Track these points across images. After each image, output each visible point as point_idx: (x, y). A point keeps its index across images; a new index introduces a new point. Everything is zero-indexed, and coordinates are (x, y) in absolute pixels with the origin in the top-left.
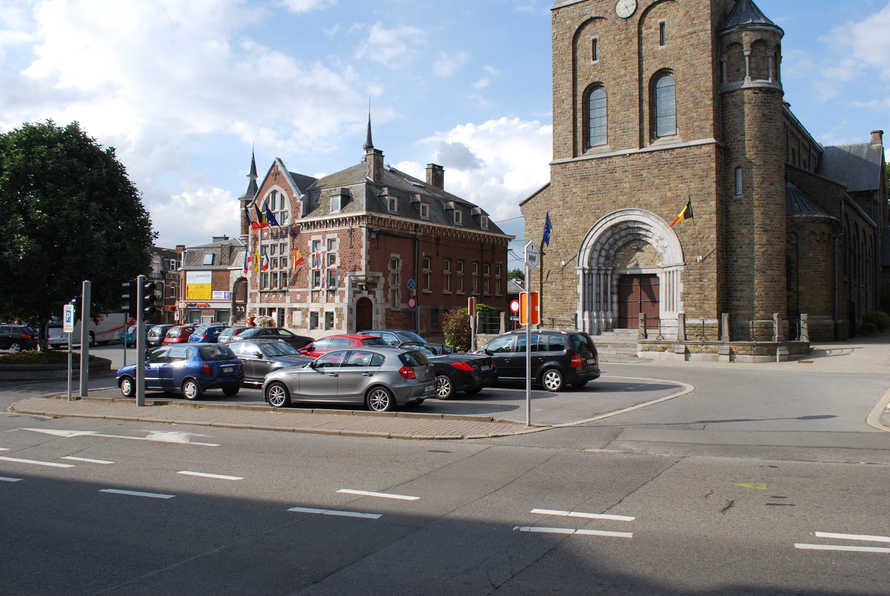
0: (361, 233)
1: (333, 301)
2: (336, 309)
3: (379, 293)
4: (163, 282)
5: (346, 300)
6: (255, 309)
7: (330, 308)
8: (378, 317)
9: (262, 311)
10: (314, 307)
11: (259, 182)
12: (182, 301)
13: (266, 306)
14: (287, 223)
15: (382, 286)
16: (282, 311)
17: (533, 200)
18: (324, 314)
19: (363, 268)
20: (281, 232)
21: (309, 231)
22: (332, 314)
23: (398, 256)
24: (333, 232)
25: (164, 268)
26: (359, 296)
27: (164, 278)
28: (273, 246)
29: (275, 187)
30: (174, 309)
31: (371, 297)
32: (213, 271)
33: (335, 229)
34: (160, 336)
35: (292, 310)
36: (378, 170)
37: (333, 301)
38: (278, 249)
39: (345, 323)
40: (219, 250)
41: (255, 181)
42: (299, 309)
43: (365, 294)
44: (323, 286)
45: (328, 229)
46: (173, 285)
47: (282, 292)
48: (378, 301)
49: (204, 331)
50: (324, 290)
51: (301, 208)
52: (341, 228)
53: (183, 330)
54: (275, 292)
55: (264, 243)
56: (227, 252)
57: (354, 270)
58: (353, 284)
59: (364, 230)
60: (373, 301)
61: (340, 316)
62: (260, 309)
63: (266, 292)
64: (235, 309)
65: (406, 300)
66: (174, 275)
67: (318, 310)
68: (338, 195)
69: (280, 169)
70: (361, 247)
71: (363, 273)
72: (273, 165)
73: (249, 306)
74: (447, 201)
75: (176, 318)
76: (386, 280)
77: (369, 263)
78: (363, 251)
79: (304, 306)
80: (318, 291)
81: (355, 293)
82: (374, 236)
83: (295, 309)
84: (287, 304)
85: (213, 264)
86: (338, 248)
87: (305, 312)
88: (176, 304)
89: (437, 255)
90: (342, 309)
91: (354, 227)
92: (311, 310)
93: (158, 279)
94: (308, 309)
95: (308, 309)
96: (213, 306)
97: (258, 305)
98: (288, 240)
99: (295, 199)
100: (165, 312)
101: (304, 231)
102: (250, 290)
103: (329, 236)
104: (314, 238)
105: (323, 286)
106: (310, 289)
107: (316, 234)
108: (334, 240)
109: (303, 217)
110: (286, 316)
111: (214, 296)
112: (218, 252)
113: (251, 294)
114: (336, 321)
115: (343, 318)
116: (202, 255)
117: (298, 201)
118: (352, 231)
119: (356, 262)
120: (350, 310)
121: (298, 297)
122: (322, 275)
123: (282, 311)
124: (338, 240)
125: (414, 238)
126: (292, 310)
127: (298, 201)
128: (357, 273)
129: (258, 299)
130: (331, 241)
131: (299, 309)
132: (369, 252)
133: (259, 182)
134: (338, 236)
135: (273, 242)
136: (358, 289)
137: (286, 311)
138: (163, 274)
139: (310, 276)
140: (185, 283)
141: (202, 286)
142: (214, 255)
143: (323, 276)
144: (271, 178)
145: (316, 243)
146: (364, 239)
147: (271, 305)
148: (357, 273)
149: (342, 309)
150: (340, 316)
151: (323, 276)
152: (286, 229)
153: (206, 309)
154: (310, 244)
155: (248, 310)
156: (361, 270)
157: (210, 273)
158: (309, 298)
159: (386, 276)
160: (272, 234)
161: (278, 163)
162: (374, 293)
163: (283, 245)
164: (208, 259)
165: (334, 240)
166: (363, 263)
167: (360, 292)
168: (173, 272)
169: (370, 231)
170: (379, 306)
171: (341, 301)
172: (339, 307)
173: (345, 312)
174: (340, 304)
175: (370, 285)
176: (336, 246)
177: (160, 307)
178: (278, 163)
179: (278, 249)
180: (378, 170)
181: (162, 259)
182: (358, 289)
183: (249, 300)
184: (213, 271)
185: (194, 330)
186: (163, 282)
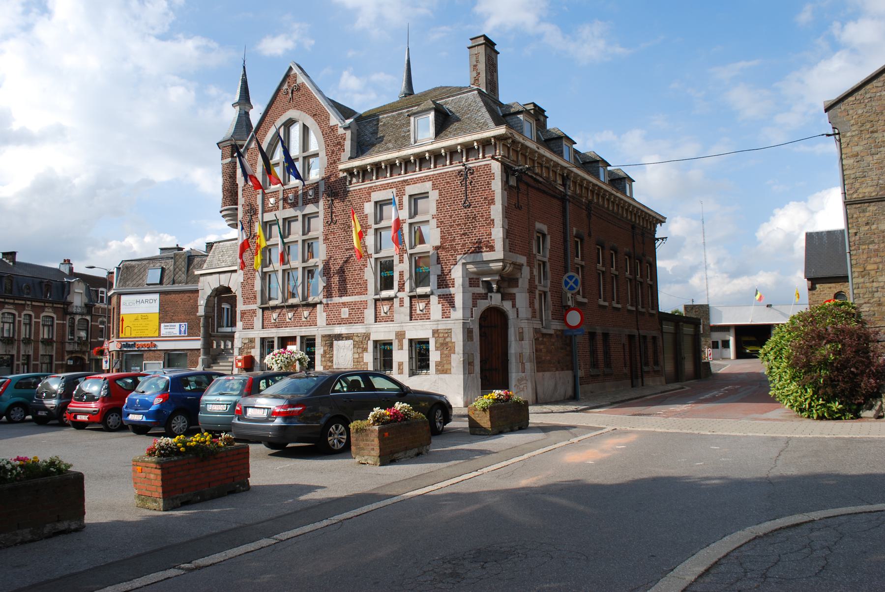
0: (491, 176)
1: (426, 316)
2: (435, 332)
3: (522, 298)
4: (88, 318)
5: (458, 314)
6: (252, 341)
7: (419, 330)
8: (520, 347)
9: (267, 345)
10: (382, 332)
11: (255, 117)
12: (114, 339)
13: (274, 333)
14: (315, 175)
15: (527, 286)
16: (309, 343)
17: (858, 95)
18: (406, 343)
19: (499, 245)
20: (305, 194)
21: (367, 184)
22: (427, 342)
23: (544, 228)
24: (420, 181)
25: (90, 299)
26: (483, 304)
27: (89, 312)
28: (288, 221)
29: (292, 114)
30: (102, 353)
31: (507, 306)
32: (161, 293)
33: (425, 173)
34: (61, 397)
35: (331, 340)
36: (492, 75)
37: (426, 316)
38: (297, 227)
39: (457, 360)
40: (171, 262)
41: (247, 114)
42: (348, 337)
43: (496, 299)
44: (401, 288)
45: (408, 177)
46: (102, 323)
47: (308, 305)
48: (520, 314)
49: (162, 385)
50: (405, 295)
51: (348, 144)
52: (441, 170)
53: (112, 384)
54: (292, 307)
55: (268, 217)
56: (183, 264)
57: (478, 250)
58: (472, 281)
59: (496, 167)
60: (511, 314)
61: (445, 346)
62: (263, 340)
63: (274, 308)
64: (207, 346)
65: (561, 311)
66: (104, 309)
67: (391, 336)
68: (430, 109)
69: (301, 79)
70: (492, 202)
71: (499, 253)
72: (287, 76)
73: (240, 334)
74: (511, 187)
75: (105, 366)
76: (531, 273)
77: (508, 234)
78: (497, 211)
79: (358, 329)
80: (390, 299)
81: (476, 297)
82: (513, 182)
83: (339, 337)
84: (320, 328)
85: (161, 283)
86: (433, 210)
87: (360, 342)
88: (105, 346)
89: (590, 235)
90: (449, 332)
91: (472, 164)
92: (373, 337)
93: (82, 314)
94: (367, 336)
95: (367, 336)
96: (161, 346)
97: (258, 333)
98: (321, 207)
99: (333, 129)
100: (90, 360)
101: (356, 186)
102: (240, 307)
103: (411, 190)
104: (377, 196)
105: (401, 288)
106: (371, 296)
107: (381, 189)
108: (425, 195)
109: (350, 158)
110: (319, 351)
111: (164, 331)
112: (170, 265)
113: (243, 313)
114: (434, 356)
115: (452, 350)
116: (145, 269)
117: (341, 131)
118: (466, 175)
119: (479, 233)
120: (468, 333)
121: (345, 313)
122: (398, 268)
123: (309, 343)
124: (434, 195)
125: (563, 199)
126: (331, 340)
127: (341, 131)
128: (487, 256)
129: (258, 322)
130: (415, 199)
131: (348, 337)
132: (508, 212)
133: (255, 117)
134: (434, 187)
135: (290, 212)
136: (481, 290)
137: (318, 341)
138: (89, 308)
139: (370, 275)
140: (119, 313)
141: (145, 317)
142: (163, 270)
143: (402, 268)
144: (282, 99)
145: (380, 205)
146: (497, 185)
147: (286, 332)
148: (487, 256)
149: (449, 332)
150: (445, 346)
151: (402, 268)
152: (316, 186)
153: (151, 351)
154: (369, 208)
155: (238, 343)
156: (492, 248)
157: (157, 297)
158: (369, 313)
159: (530, 264)
160: (285, 200)
161: (296, 70)
162: (512, 298)
163: (307, 218)
164: (153, 276)
165: (425, 195)
166: (497, 234)
167: (485, 297)
168: (102, 305)
169: (507, 170)
170: (524, 325)
171: (445, 315)
172: (441, 327)
173: (458, 338)
174: (445, 322)
175: (507, 281)
176: (429, 207)
177: (84, 353)
178: (296, 70)
179: (297, 227)
180: (492, 75)
181: (88, 289)
182: (481, 290)
183: (239, 324)
184: (161, 293)
185: (136, 383)
186: (88, 318)
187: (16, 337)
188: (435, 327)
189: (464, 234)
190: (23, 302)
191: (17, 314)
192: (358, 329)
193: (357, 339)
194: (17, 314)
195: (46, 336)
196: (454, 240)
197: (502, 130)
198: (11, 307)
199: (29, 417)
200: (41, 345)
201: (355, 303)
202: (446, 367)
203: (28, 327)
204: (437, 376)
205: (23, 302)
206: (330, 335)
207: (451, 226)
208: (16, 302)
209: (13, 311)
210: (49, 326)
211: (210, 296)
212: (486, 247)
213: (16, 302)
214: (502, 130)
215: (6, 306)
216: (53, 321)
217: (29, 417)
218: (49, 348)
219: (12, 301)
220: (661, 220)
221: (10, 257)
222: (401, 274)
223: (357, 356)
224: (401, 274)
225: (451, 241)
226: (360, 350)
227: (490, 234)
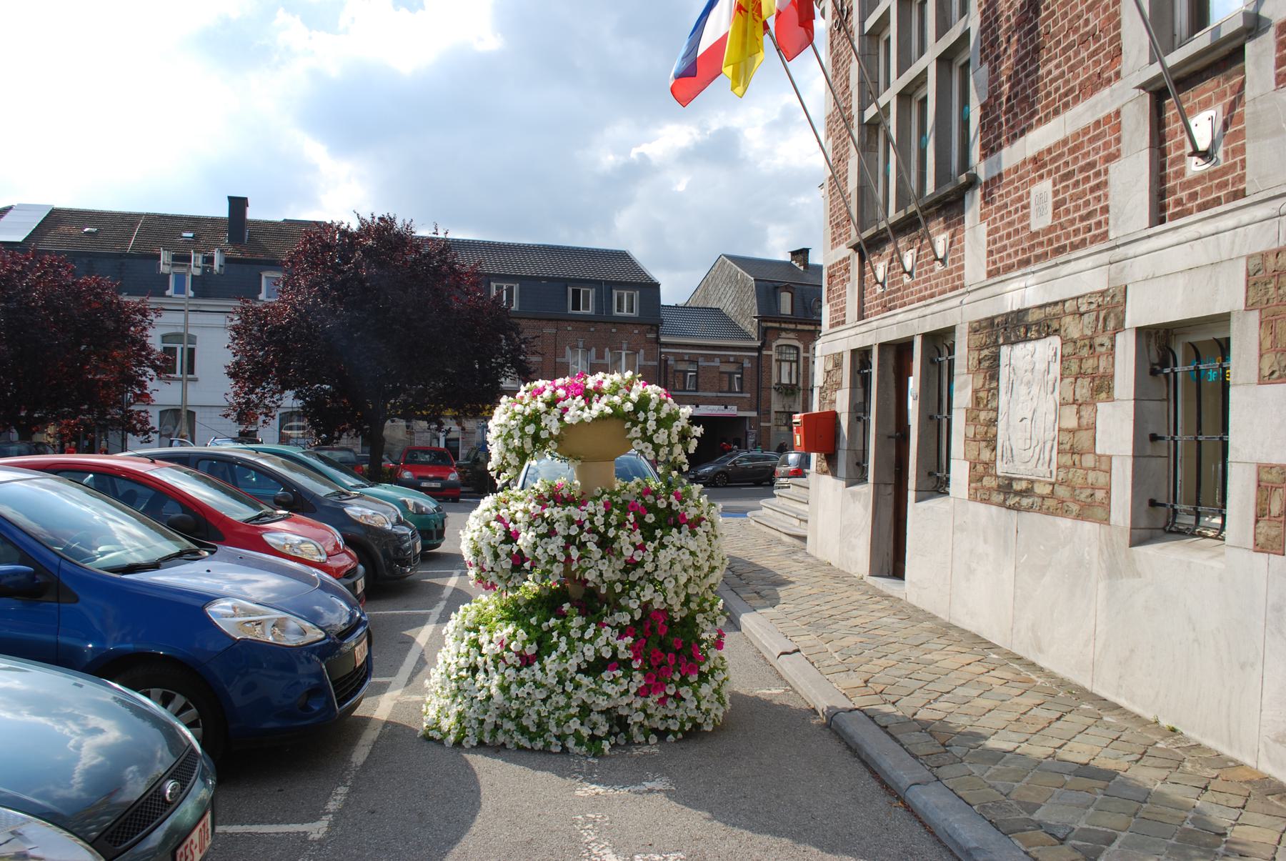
79: (1081, 276)
92: (1147, 308)
94: (1110, 306)
95: (1110, 306)
187: (801, 385)
190: (777, 325)
191: (801, 346)
192: (1081, 276)
193: (1074, 329)
194: (801, 346)
195: (785, 380)
198: (792, 335)
199: (407, 475)
200: (774, 394)
201: (1072, 145)
203: (794, 365)
205: (777, 325)
206: (991, 321)
208: (799, 327)
209: (796, 343)
210: (791, 362)
213: (799, 327)
215: (783, 334)
216: (798, 354)
217: (407, 475)
218: (788, 401)
219: (792, 326)
221: (801, 257)
223: (1071, 422)
226: (1083, 389)
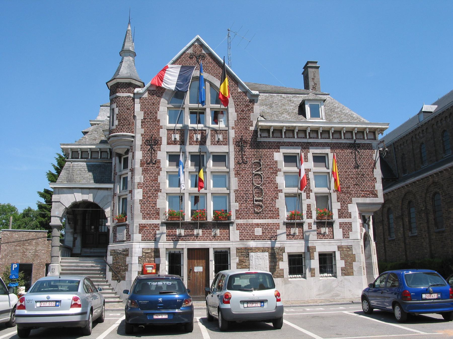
2: (339, 248)
7: (323, 246)
90: (350, 248)
114: (340, 264)
121: (258, 231)
171: (346, 235)
172: (345, 243)
188: (339, 244)
189: (357, 184)
196: (349, 187)
197: (270, 273)
201: (268, 225)
202: (349, 271)
204: (343, 277)
207: (346, 178)
211: (365, 291)
212: (372, 194)
214: (270, 273)
220: (283, 261)
222: (309, 206)
224: (309, 206)
225: (347, 188)
227: (374, 186)
